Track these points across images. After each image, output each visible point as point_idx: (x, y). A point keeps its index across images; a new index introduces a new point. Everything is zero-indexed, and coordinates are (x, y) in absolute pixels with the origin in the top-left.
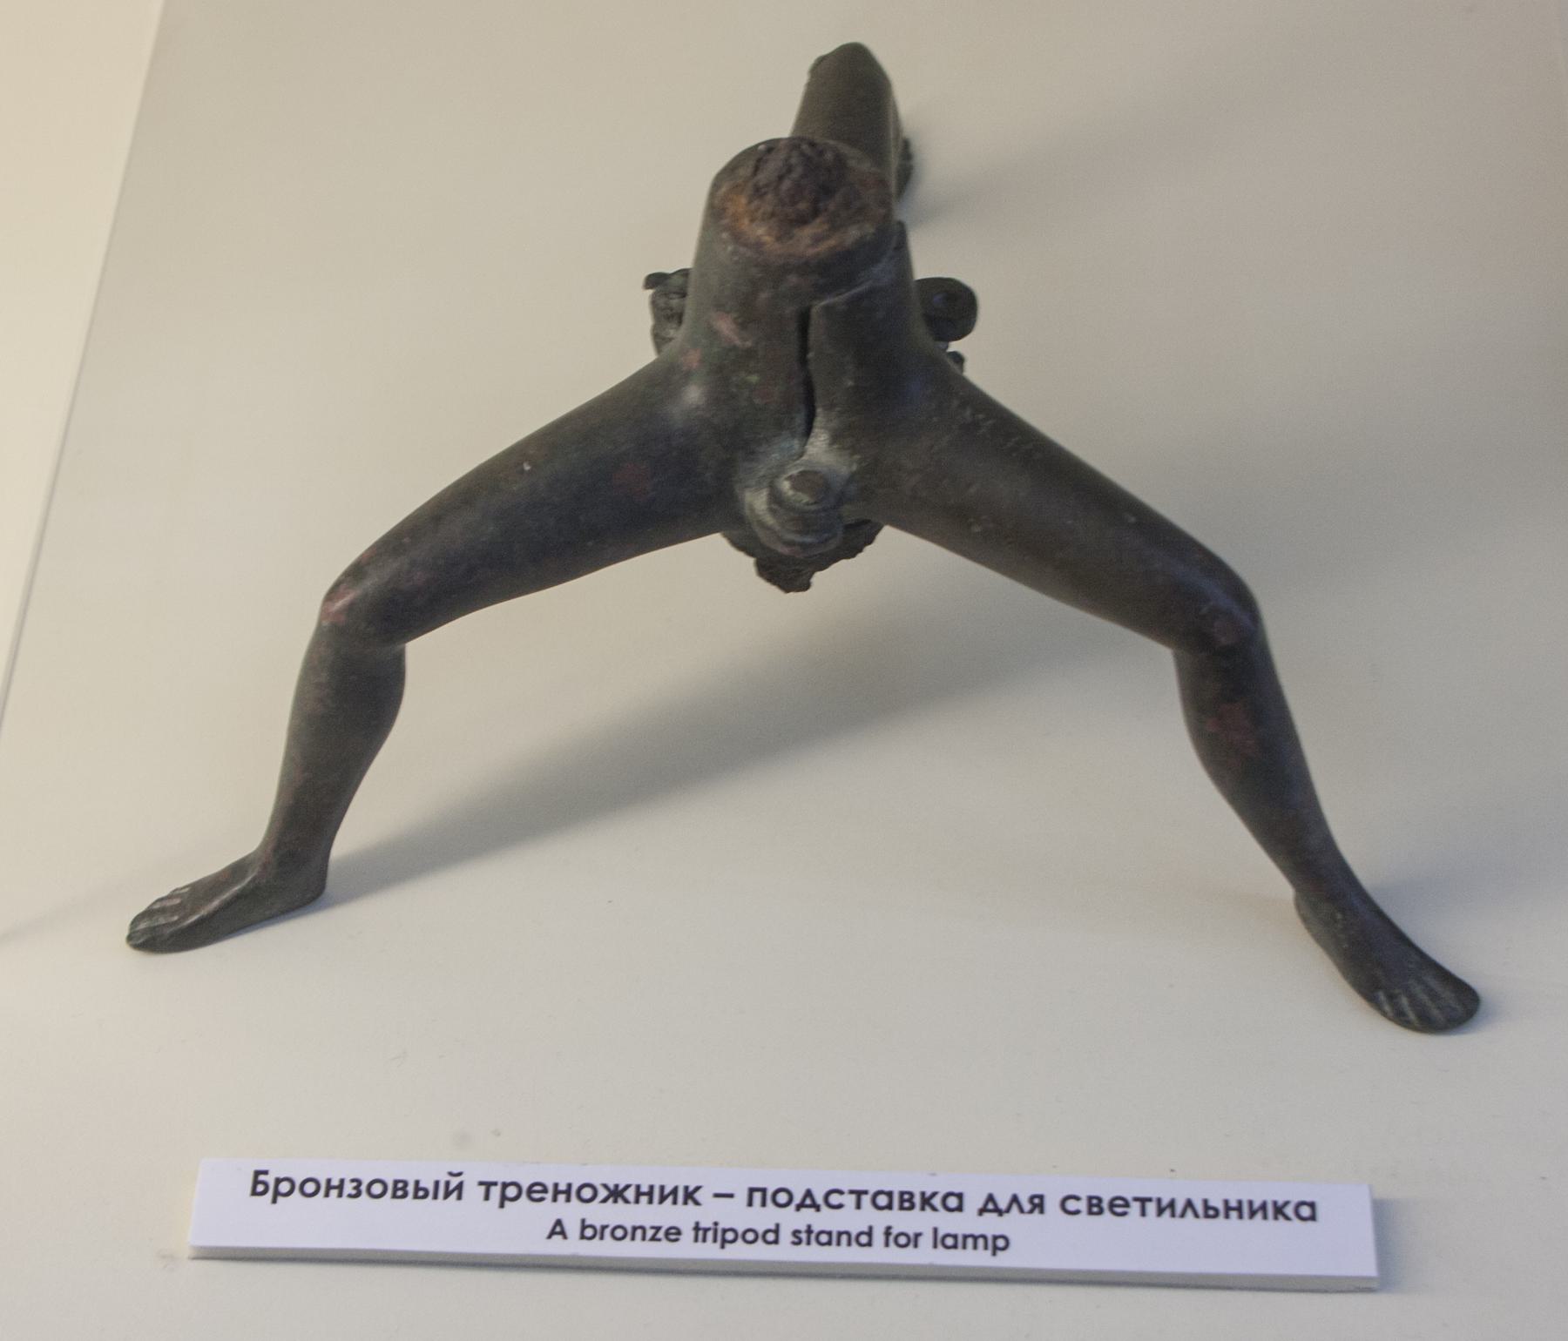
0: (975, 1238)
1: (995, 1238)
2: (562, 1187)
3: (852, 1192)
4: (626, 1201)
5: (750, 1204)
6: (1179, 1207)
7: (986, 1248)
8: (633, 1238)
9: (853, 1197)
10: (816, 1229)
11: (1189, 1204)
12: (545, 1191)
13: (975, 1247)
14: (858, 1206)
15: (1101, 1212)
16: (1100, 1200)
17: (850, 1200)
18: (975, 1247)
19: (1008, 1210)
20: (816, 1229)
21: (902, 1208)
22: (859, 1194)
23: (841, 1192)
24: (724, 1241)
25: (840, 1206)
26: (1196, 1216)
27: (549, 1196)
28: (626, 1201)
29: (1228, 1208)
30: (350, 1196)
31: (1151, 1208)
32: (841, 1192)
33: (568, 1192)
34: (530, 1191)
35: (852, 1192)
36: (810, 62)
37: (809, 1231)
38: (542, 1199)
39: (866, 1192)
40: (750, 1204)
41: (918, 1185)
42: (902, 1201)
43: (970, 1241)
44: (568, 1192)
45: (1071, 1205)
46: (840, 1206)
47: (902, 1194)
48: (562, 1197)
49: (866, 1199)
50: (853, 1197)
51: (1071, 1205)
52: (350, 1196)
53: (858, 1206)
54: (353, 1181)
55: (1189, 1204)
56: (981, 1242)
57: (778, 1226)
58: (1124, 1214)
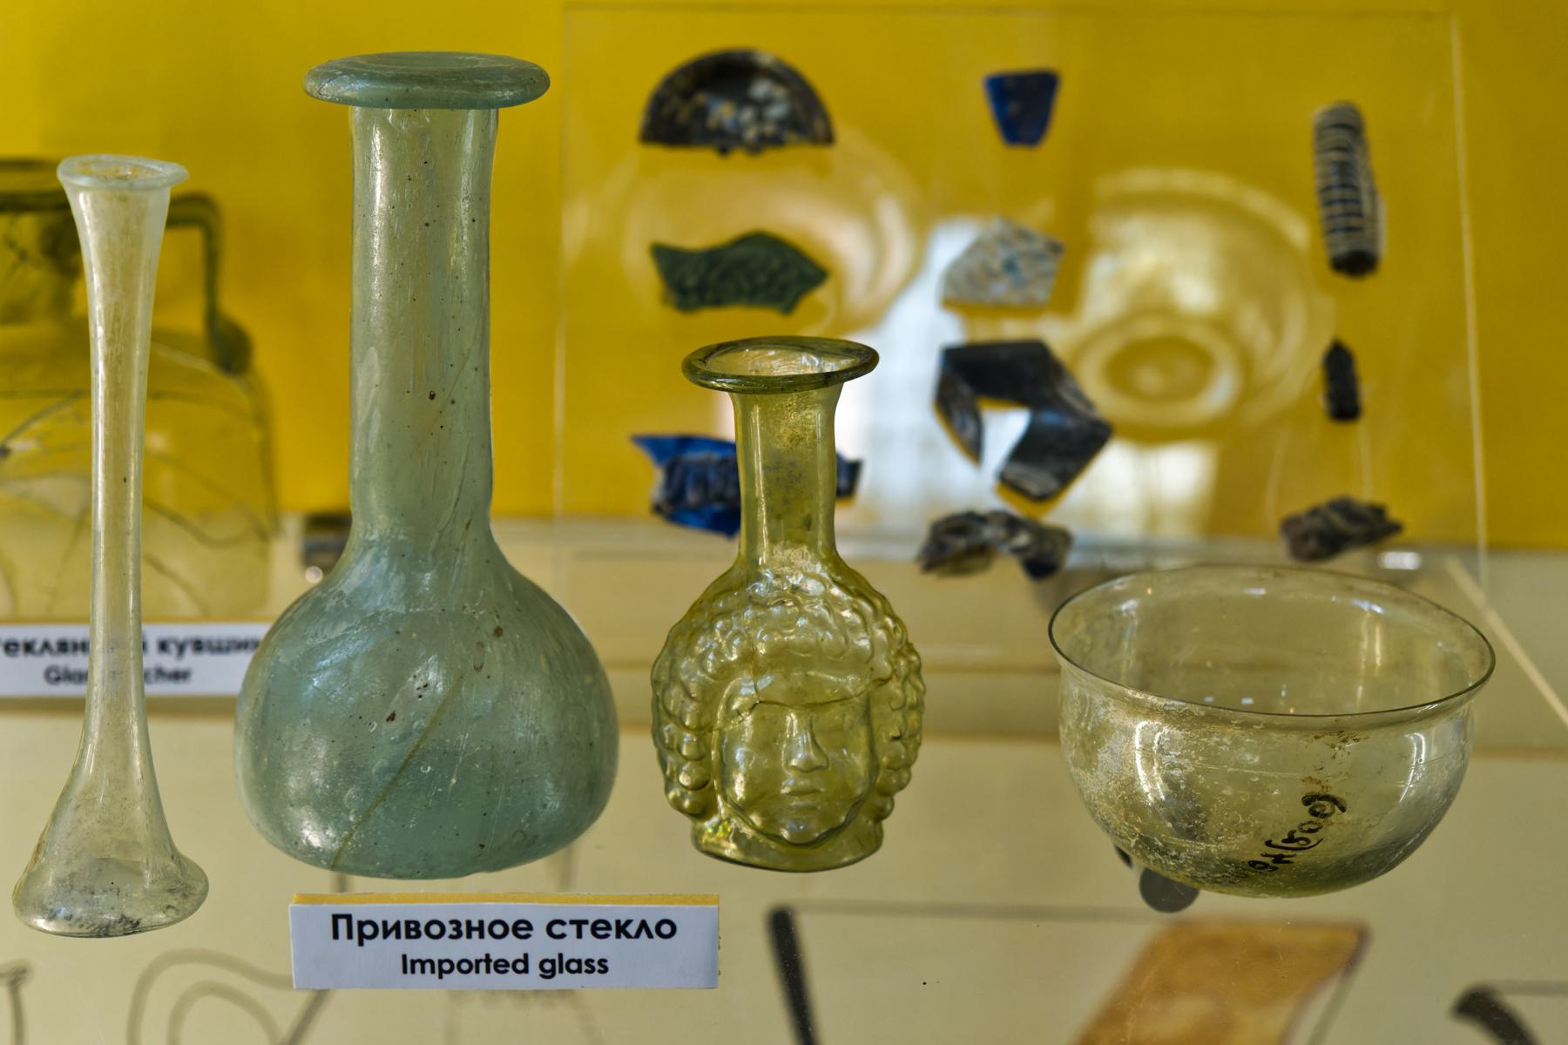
0: (423, 963)
1: (441, 962)
2: (475, 924)
3: (572, 922)
4: (628, 936)
5: (336, 936)
6: (632, 929)
7: (433, 971)
8: (477, 971)
9: (574, 927)
10: (494, 958)
11: (643, 925)
12: (609, 927)
13: (423, 971)
14: (579, 935)
15: (418, 935)
16: (417, 924)
17: (571, 930)
18: (423, 971)
19: (638, 935)
20: (494, 958)
21: (408, 936)
22: (579, 924)
23: (562, 923)
24: (442, 972)
25: (563, 936)
26: (650, 936)
27: (613, 933)
28: (628, 936)
29: (470, 929)
30: (451, 937)
31: (586, 929)
32: (562, 923)
33: (480, 929)
34: (516, 928)
35: (572, 922)
36: (681, 374)
37: (488, 959)
38: (607, 936)
39: (586, 922)
40: (336, 936)
41: (633, 912)
42: (408, 930)
43: (418, 966)
44: (480, 929)
45: (557, 929)
46: (563, 936)
47: (408, 923)
48: (475, 934)
49: (586, 929)
50: (574, 927)
51: (557, 929)
52: (451, 937)
53: (579, 935)
54: (452, 922)
55: (643, 925)
56: (428, 966)
57: (526, 956)
58: (528, 936)
